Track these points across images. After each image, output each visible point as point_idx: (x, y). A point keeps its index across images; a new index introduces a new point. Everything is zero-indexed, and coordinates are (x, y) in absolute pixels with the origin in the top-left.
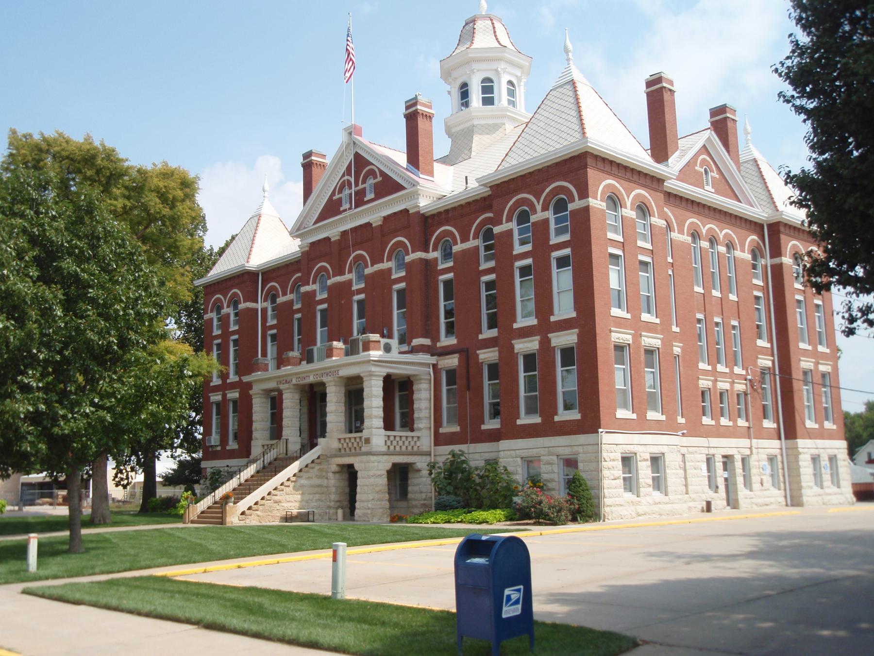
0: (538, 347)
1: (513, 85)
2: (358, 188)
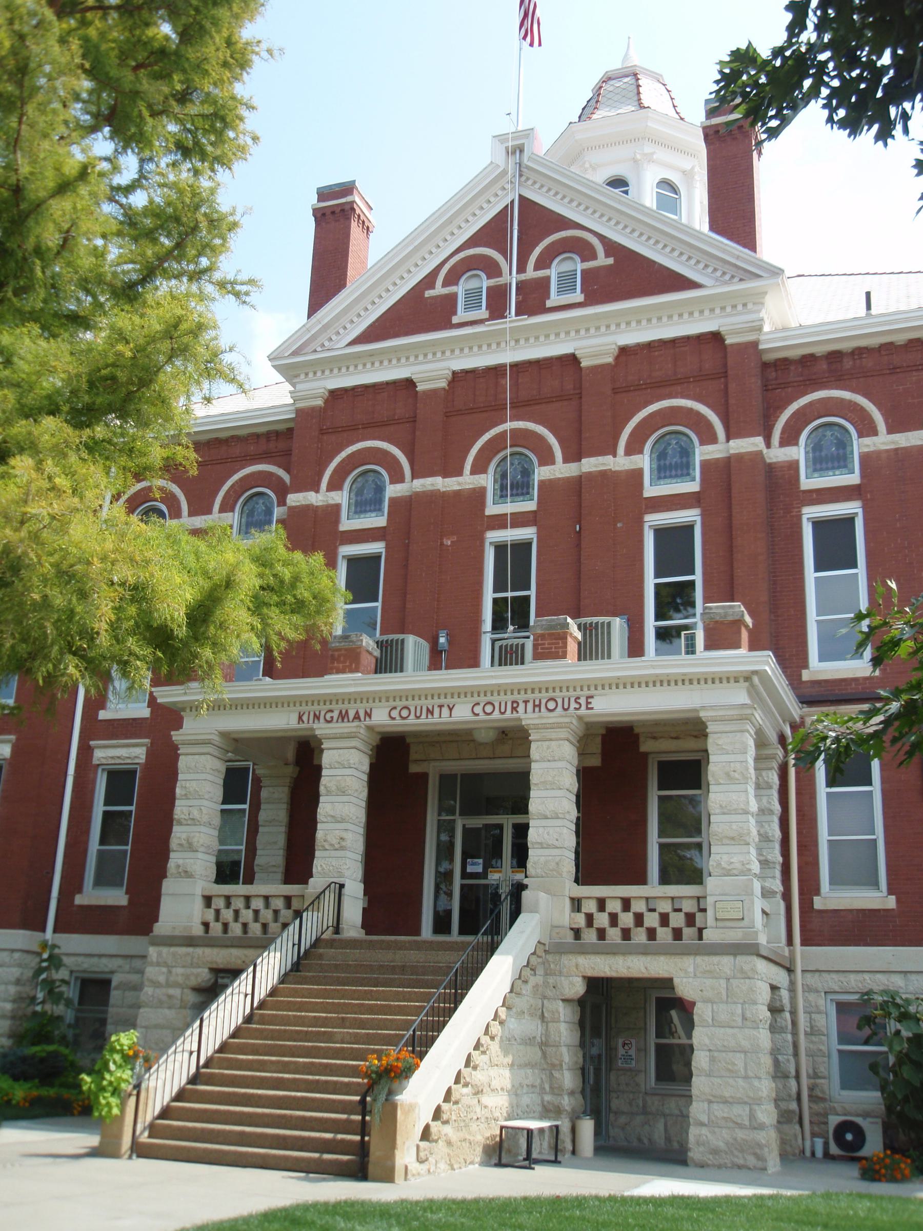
0: (142, 759)
1: (674, 189)
2: (523, 277)
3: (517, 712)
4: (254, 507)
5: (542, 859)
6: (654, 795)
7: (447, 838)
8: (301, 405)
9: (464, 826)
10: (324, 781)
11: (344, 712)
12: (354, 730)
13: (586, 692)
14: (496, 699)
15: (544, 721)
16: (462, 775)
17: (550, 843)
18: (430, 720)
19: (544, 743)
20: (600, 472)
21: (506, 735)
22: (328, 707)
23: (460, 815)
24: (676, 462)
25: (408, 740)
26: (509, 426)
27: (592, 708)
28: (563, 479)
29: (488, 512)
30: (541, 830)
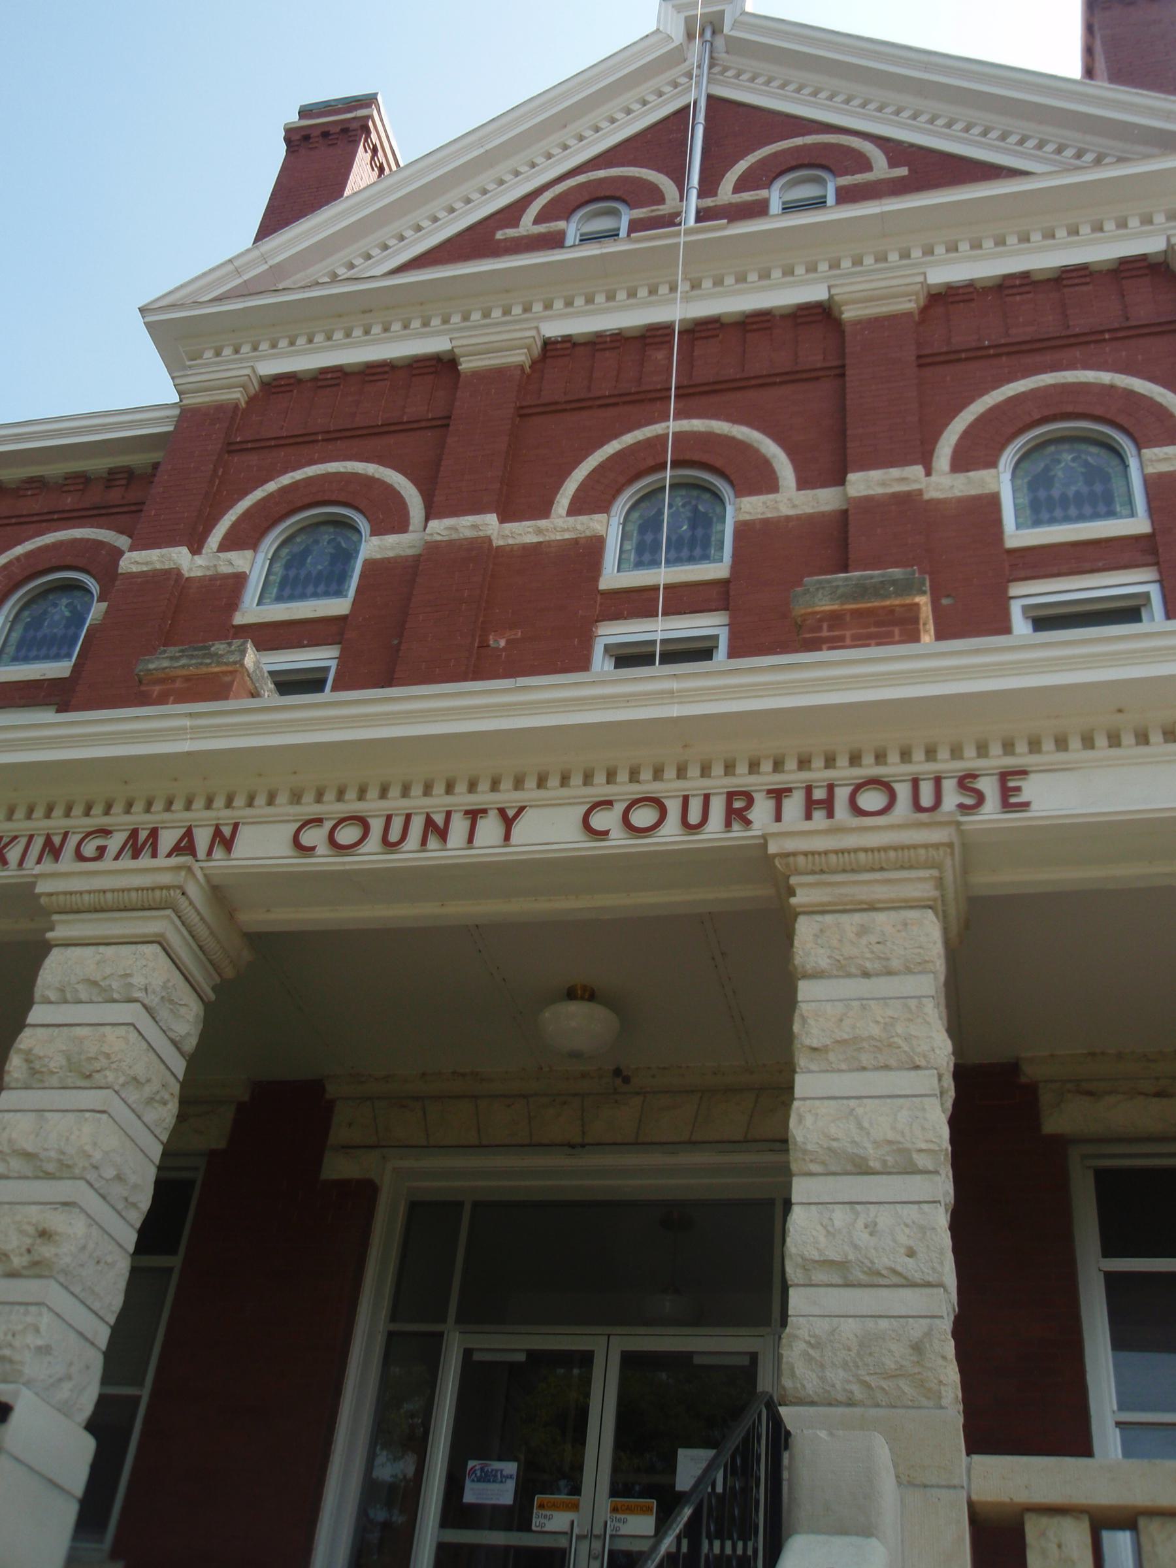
3: (748, 822)
4: (45, 612)
5: (849, 1328)
6: (1093, 1271)
7: (371, 1513)
8: (192, 400)
9: (468, 1353)
10: (27, 1040)
11: (143, 835)
12: (166, 879)
13: (998, 760)
14: (669, 788)
15: (850, 841)
16: (476, 1205)
17: (882, 1262)
18: (435, 854)
19: (844, 918)
20: (895, 496)
21: (626, 1080)
22: (98, 820)
23: (458, 1321)
24: (1077, 493)
25: (331, 1090)
26: (673, 426)
27: (1025, 805)
28: (798, 518)
29: (605, 584)
30: (840, 1217)
